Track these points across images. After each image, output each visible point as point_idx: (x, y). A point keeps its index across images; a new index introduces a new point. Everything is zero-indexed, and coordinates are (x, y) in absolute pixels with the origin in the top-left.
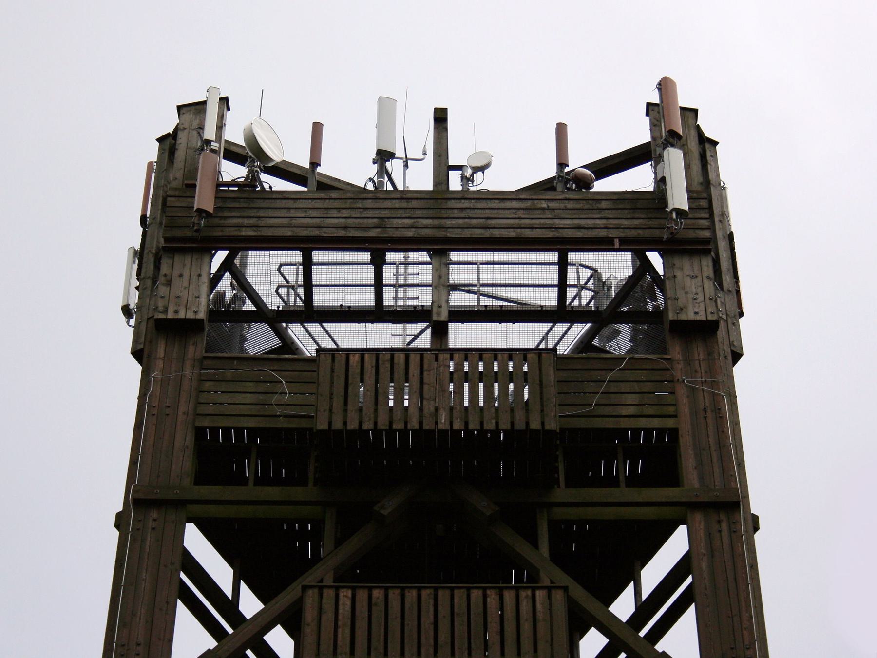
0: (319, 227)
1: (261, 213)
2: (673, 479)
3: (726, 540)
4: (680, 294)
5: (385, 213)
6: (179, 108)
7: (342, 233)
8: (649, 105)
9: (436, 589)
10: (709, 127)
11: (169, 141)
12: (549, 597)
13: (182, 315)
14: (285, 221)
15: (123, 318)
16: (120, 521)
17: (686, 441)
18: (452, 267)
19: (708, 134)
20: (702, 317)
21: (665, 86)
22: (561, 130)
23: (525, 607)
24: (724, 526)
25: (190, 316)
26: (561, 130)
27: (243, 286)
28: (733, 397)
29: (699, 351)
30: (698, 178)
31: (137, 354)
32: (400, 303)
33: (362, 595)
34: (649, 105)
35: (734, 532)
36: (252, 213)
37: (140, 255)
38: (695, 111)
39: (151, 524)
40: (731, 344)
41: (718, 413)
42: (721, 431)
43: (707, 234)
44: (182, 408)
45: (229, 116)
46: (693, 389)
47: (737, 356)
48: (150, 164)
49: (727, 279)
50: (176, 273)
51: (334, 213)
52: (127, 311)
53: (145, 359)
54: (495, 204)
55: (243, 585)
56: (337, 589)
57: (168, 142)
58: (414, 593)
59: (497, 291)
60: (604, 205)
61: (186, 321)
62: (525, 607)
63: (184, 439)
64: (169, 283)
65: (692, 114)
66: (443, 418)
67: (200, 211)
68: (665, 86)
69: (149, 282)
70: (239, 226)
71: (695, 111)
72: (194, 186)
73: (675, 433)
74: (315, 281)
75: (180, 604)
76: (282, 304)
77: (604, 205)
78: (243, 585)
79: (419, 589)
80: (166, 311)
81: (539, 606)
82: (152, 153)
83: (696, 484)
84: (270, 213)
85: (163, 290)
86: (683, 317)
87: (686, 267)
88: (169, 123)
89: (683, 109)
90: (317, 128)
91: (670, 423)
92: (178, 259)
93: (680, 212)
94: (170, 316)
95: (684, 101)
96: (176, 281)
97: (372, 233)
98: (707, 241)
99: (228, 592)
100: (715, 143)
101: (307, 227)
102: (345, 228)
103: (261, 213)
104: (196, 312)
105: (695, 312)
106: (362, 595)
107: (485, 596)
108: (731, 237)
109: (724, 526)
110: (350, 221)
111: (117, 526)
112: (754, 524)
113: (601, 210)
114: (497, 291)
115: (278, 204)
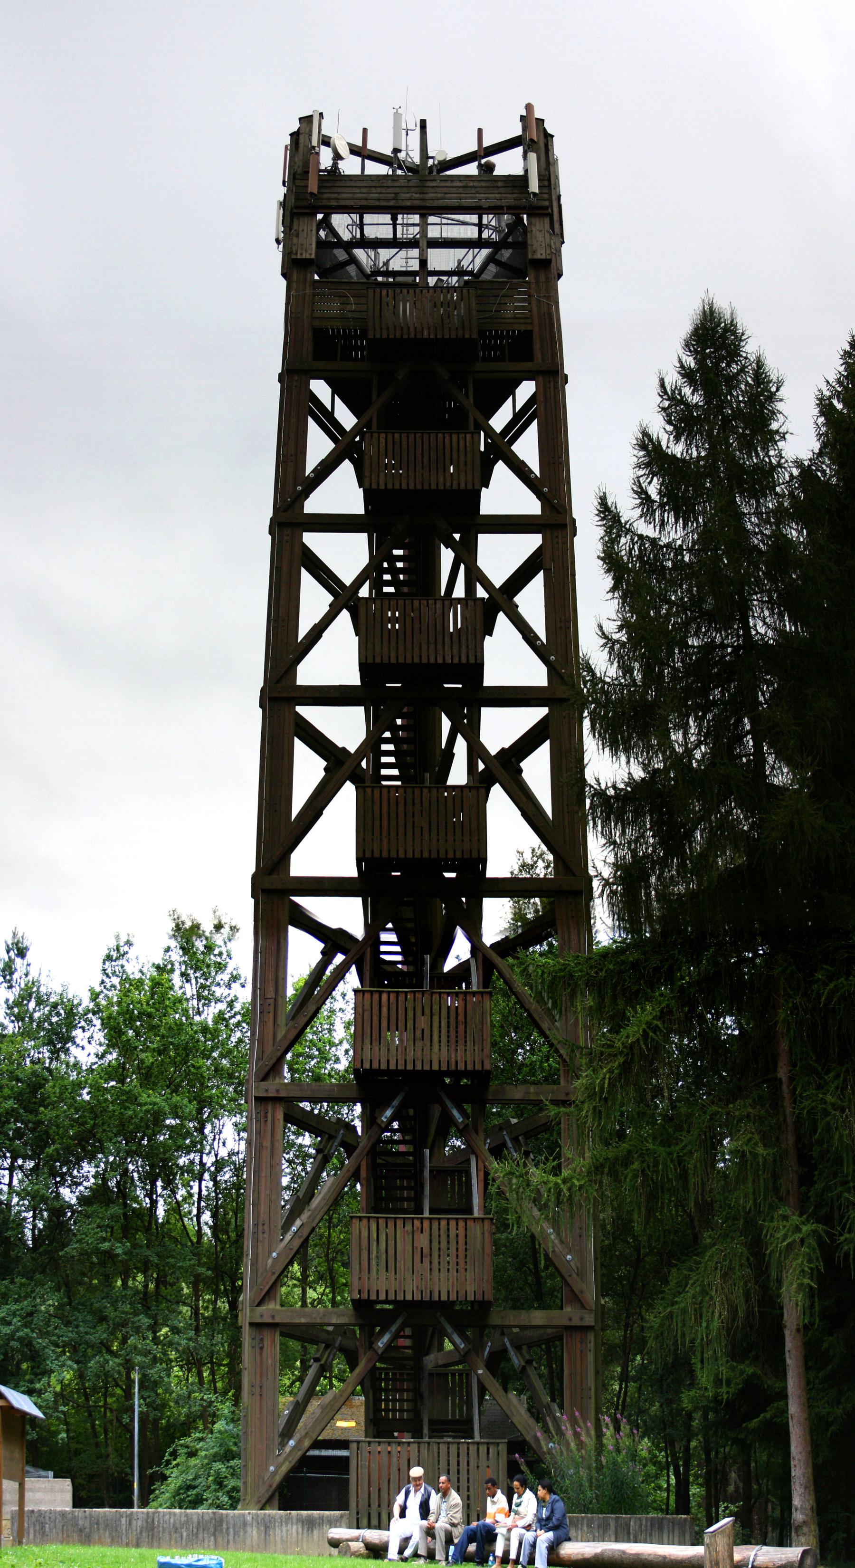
0: (366, 199)
1: (340, 190)
2: (529, 357)
3: (552, 393)
4: (534, 242)
5: (397, 190)
6: (300, 119)
7: (377, 203)
8: (522, 117)
9: (422, 433)
10: (549, 128)
11: (295, 136)
12: (472, 437)
13: (304, 257)
14: (350, 195)
15: (276, 245)
16: (281, 378)
17: (536, 336)
18: (429, 227)
19: (550, 131)
20: (543, 257)
21: (529, 107)
22: (480, 131)
23: (462, 443)
24: (552, 384)
25: (308, 257)
26: (480, 131)
27: (333, 231)
28: (557, 303)
29: (542, 276)
30: (544, 166)
31: (284, 275)
32: (405, 236)
33: (390, 437)
34: (522, 117)
35: (556, 383)
36: (335, 190)
37: (283, 205)
38: (543, 120)
39: (295, 383)
40: (558, 269)
41: (550, 314)
42: (552, 332)
43: (547, 203)
44: (306, 314)
45: (324, 122)
46: (539, 301)
47: (560, 275)
48: (286, 146)
49: (557, 226)
50: (301, 229)
51: (374, 190)
52: (278, 241)
53: (297, 551)
54: (449, 184)
55: (336, 397)
56: (379, 433)
57: (295, 136)
58: (413, 435)
59: (450, 222)
60: (500, 184)
61: (306, 260)
62: (462, 443)
63: (308, 335)
64: (297, 236)
65: (541, 122)
66: (426, 333)
67: (311, 193)
68: (529, 107)
69: (288, 229)
70: (329, 199)
71: (543, 120)
72: (308, 172)
73: (530, 332)
74: (365, 222)
75: (310, 418)
76: (350, 236)
77: (500, 184)
78: (336, 397)
79: (415, 434)
80: (296, 254)
81: (468, 444)
82: (287, 141)
83: (540, 360)
84: (344, 190)
85: (295, 240)
86: (535, 257)
87: (536, 221)
88: (295, 126)
89: (537, 119)
90: (365, 131)
91: (529, 328)
92: (301, 219)
93: (534, 194)
94: (299, 257)
95: (538, 115)
96: (301, 234)
97: (392, 203)
98: (546, 208)
99: (329, 407)
100: (552, 136)
101: (361, 199)
102: (379, 200)
103: (340, 190)
104: (310, 254)
105: (541, 254)
106: (390, 437)
107: (444, 437)
108: (559, 196)
109: (552, 384)
110: (381, 195)
111: (279, 381)
112: (565, 379)
113: (498, 187)
114: (450, 222)
115: (348, 184)
